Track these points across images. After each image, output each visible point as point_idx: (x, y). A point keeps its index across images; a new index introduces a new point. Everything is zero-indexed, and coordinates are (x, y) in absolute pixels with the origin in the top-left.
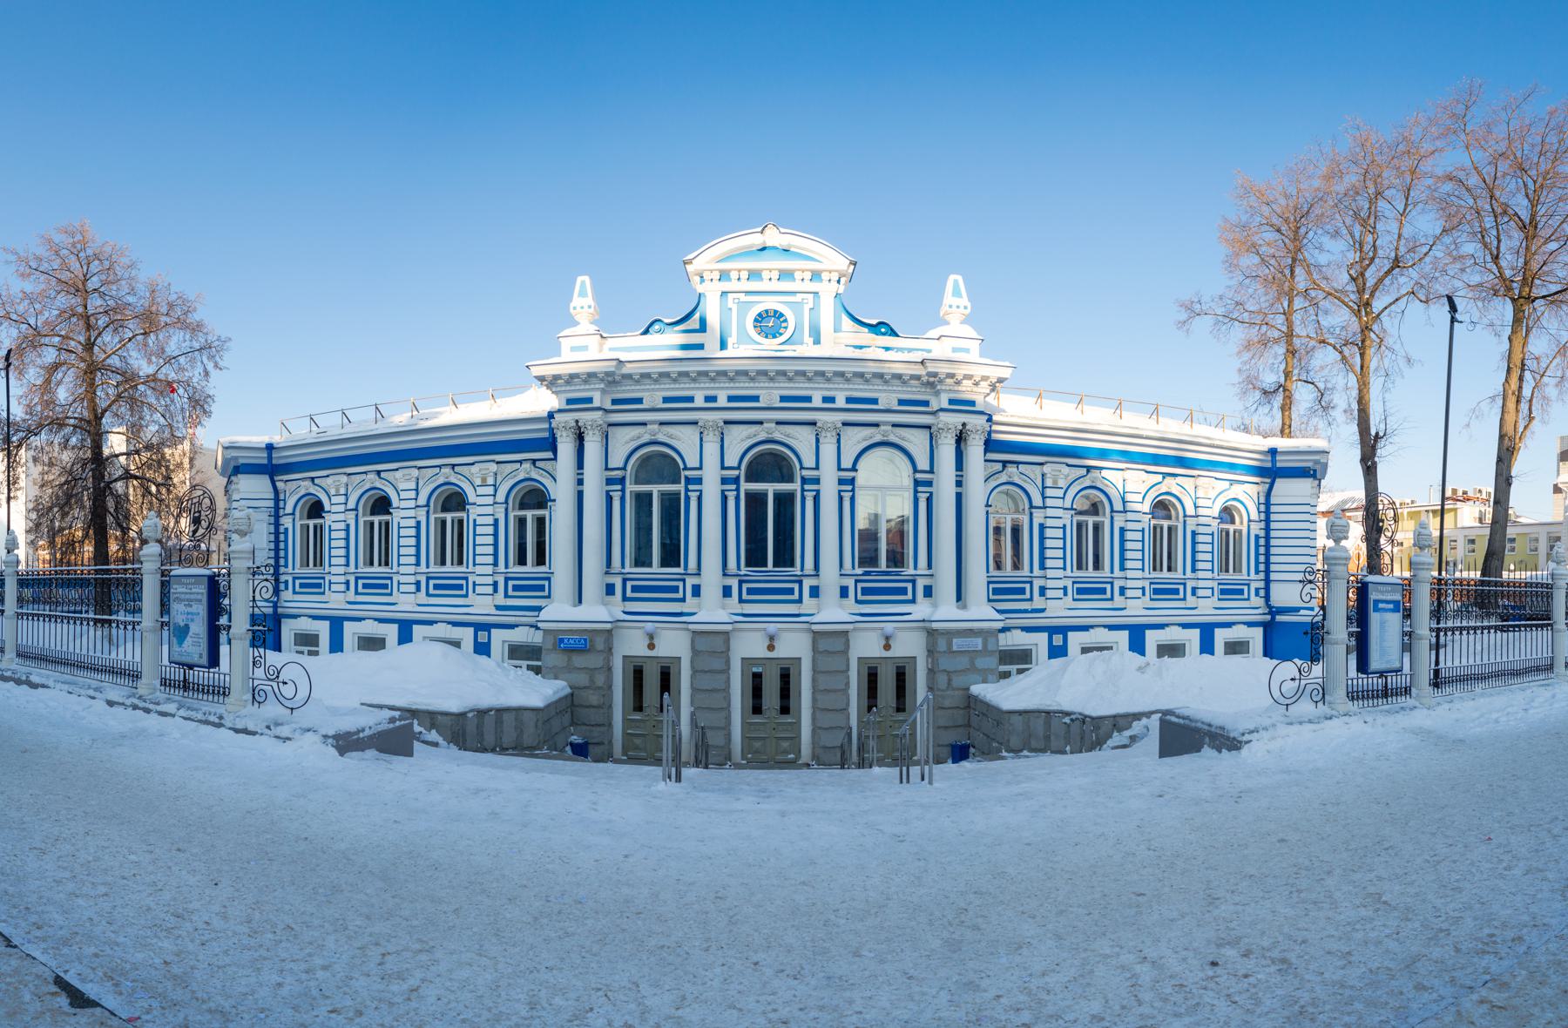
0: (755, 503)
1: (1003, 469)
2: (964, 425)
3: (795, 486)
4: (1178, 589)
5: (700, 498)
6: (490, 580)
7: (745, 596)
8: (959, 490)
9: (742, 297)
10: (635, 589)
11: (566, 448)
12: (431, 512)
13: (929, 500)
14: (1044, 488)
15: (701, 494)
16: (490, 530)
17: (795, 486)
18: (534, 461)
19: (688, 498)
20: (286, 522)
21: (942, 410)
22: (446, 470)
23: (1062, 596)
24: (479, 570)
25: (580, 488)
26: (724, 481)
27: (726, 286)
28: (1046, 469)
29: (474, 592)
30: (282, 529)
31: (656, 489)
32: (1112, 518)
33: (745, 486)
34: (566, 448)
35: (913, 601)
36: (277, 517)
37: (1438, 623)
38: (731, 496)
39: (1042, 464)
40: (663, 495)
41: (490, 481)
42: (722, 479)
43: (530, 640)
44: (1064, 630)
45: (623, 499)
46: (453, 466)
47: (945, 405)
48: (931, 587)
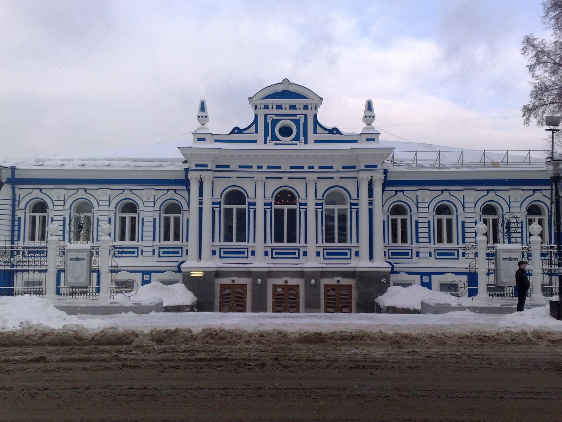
0: (279, 213)
1: (396, 194)
2: (372, 177)
3: (296, 206)
4: (347, 253)
5: (255, 212)
6: (151, 249)
7: (274, 256)
8: (371, 207)
9: (302, 121)
10: (225, 253)
11: (194, 188)
12: (117, 213)
13: (357, 212)
14: (417, 202)
15: (255, 210)
16: (152, 224)
17: (296, 206)
18: (175, 190)
19: (249, 212)
20: (20, 214)
21: (362, 170)
22: (127, 192)
23: (428, 256)
24: (145, 244)
25: (201, 206)
26: (266, 204)
27: (266, 111)
28: (418, 193)
29: (142, 254)
30: (16, 218)
31: (235, 207)
32: (457, 216)
33: (274, 206)
34: (194, 188)
35: (350, 258)
36: (14, 210)
37: (551, 267)
38: (268, 211)
39: (416, 190)
40: (238, 210)
41: (152, 199)
42: (264, 203)
43: (172, 278)
44: (429, 274)
45: (220, 211)
46: (131, 190)
47: (363, 168)
48: (358, 252)
